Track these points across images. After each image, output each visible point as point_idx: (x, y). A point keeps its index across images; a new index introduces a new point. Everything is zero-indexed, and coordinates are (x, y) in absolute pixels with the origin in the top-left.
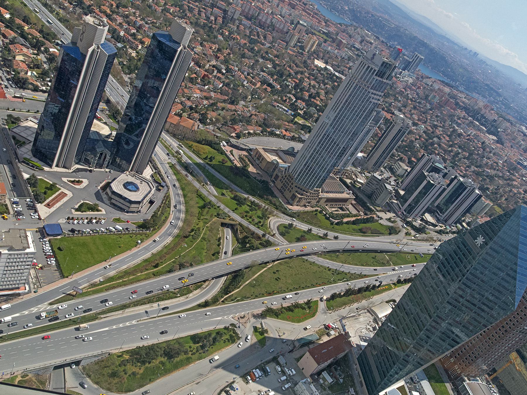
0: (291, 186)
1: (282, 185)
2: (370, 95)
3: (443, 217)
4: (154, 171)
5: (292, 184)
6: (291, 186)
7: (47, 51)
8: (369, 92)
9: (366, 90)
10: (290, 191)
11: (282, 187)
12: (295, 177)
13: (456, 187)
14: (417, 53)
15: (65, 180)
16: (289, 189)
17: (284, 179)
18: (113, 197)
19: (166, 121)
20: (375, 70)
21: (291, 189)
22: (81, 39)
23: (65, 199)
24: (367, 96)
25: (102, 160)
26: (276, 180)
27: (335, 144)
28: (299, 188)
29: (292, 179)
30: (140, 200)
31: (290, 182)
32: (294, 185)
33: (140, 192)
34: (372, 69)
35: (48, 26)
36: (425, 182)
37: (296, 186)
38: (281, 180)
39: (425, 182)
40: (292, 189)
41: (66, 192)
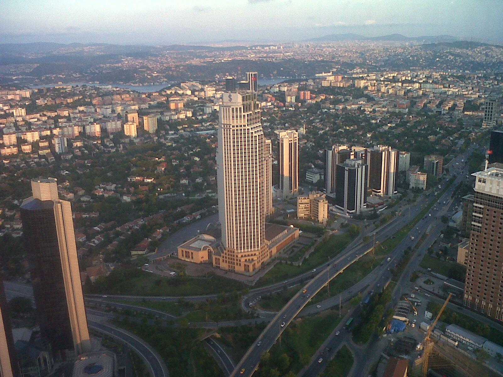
0: (237, 260)
2: (250, 131)
3: (382, 192)
4: (101, 339)
5: (237, 256)
9: (245, 130)
10: (240, 265)
11: (229, 266)
12: (235, 248)
13: (339, 159)
14: (248, 73)
16: (237, 264)
17: (226, 258)
19: (437, 295)
20: (240, 108)
21: (238, 262)
25: (43, 365)
27: (237, 117)
28: (245, 256)
29: (234, 252)
32: (239, 256)
33: (104, 369)
34: (237, 109)
36: (346, 173)
38: (223, 261)
39: (346, 173)
40: (240, 261)
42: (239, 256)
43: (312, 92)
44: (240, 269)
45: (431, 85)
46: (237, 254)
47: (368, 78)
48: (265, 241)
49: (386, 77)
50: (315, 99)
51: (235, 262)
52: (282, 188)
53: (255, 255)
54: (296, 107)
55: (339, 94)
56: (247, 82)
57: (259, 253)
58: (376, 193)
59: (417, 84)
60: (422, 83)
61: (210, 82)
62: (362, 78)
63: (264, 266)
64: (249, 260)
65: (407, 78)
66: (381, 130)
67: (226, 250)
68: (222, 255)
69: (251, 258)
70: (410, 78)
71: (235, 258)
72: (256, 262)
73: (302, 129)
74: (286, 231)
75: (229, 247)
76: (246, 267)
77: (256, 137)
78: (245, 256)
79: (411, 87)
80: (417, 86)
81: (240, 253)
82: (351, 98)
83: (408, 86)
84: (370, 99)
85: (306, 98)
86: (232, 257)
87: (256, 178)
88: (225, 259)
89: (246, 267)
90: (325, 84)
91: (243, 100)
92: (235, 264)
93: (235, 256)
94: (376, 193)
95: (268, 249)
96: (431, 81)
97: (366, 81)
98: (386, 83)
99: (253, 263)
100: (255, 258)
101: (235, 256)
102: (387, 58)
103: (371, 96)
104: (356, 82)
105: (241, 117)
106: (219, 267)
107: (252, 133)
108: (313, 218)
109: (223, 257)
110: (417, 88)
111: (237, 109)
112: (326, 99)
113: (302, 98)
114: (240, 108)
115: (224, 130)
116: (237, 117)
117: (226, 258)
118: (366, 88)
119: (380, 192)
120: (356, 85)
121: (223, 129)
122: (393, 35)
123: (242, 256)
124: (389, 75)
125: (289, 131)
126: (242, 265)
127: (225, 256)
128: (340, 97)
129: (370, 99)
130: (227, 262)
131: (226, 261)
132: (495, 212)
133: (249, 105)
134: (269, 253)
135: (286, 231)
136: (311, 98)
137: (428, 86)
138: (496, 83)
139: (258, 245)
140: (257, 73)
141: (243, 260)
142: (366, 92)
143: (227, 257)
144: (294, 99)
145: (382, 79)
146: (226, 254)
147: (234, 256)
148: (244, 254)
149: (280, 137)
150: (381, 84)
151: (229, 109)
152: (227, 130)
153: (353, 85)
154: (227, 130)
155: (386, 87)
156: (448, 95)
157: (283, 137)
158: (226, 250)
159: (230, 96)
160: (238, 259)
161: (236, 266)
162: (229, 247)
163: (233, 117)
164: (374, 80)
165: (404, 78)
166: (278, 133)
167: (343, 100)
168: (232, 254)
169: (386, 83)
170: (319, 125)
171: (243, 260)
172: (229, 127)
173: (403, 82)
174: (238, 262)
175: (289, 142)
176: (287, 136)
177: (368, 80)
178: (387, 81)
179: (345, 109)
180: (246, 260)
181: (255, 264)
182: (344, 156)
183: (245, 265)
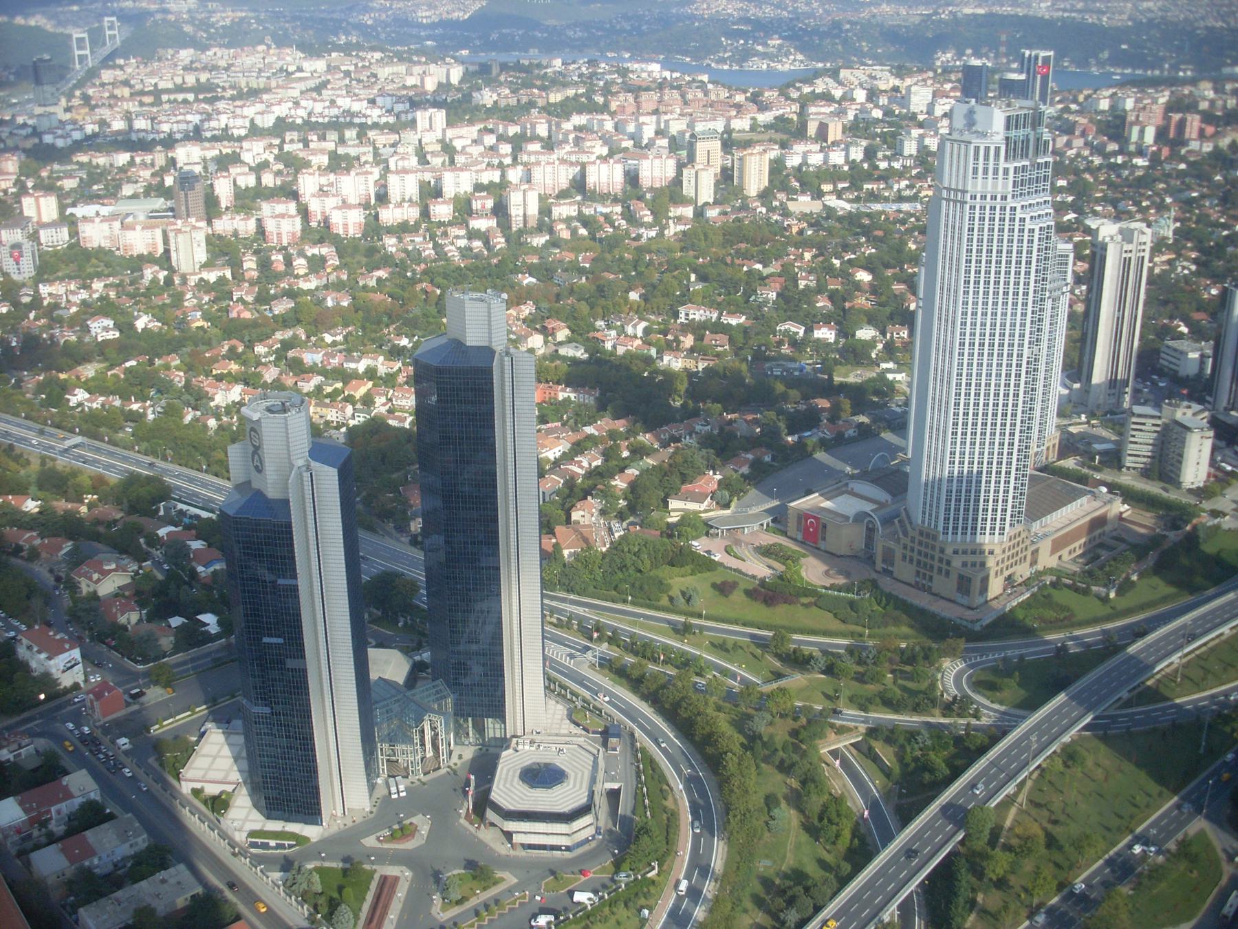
0: (941, 560)
1: (913, 568)
5: (942, 551)
6: (941, 560)
7: (153, 541)
8: (1013, 209)
10: (948, 573)
11: (918, 572)
12: (941, 529)
15: (370, 842)
16: (940, 570)
17: (912, 550)
18: (511, 826)
20: (998, 149)
21: (944, 566)
22: (256, 467)
23: (401, 893)
24: (1012, 220)
26: (892, 565)
27: (986, 171)
28: (965, 552)
30: (583, 800)
31: (919, 562)
32: (949, 551)
33: (572, 781)
34: (987, 149)
35: (148, 477)
37: (956, 552)
38: (904, 557)
40: (948, 563)
41: (392, 871)
43: (1208, 117)
51: (936, 564)
71: (937, 555)
87: (1021, 345)
88: (908, 553)
92: (935, 570)
93: (938, 549)
101: (938, 549)
109: (905, 547)
111: (987, 149)
114: (998, 149)
116: (986, 171)
126: (954, 576)
127: (910, 544)
131: (911, 560)
134: (1029, 553)
140: (1051, 53)
141: (957, 563)
143: (917, 547)
157: (1107, 239)
168: (931, 542)
174: (944, 566)
175: (1124, 255)
183: (961, 577)
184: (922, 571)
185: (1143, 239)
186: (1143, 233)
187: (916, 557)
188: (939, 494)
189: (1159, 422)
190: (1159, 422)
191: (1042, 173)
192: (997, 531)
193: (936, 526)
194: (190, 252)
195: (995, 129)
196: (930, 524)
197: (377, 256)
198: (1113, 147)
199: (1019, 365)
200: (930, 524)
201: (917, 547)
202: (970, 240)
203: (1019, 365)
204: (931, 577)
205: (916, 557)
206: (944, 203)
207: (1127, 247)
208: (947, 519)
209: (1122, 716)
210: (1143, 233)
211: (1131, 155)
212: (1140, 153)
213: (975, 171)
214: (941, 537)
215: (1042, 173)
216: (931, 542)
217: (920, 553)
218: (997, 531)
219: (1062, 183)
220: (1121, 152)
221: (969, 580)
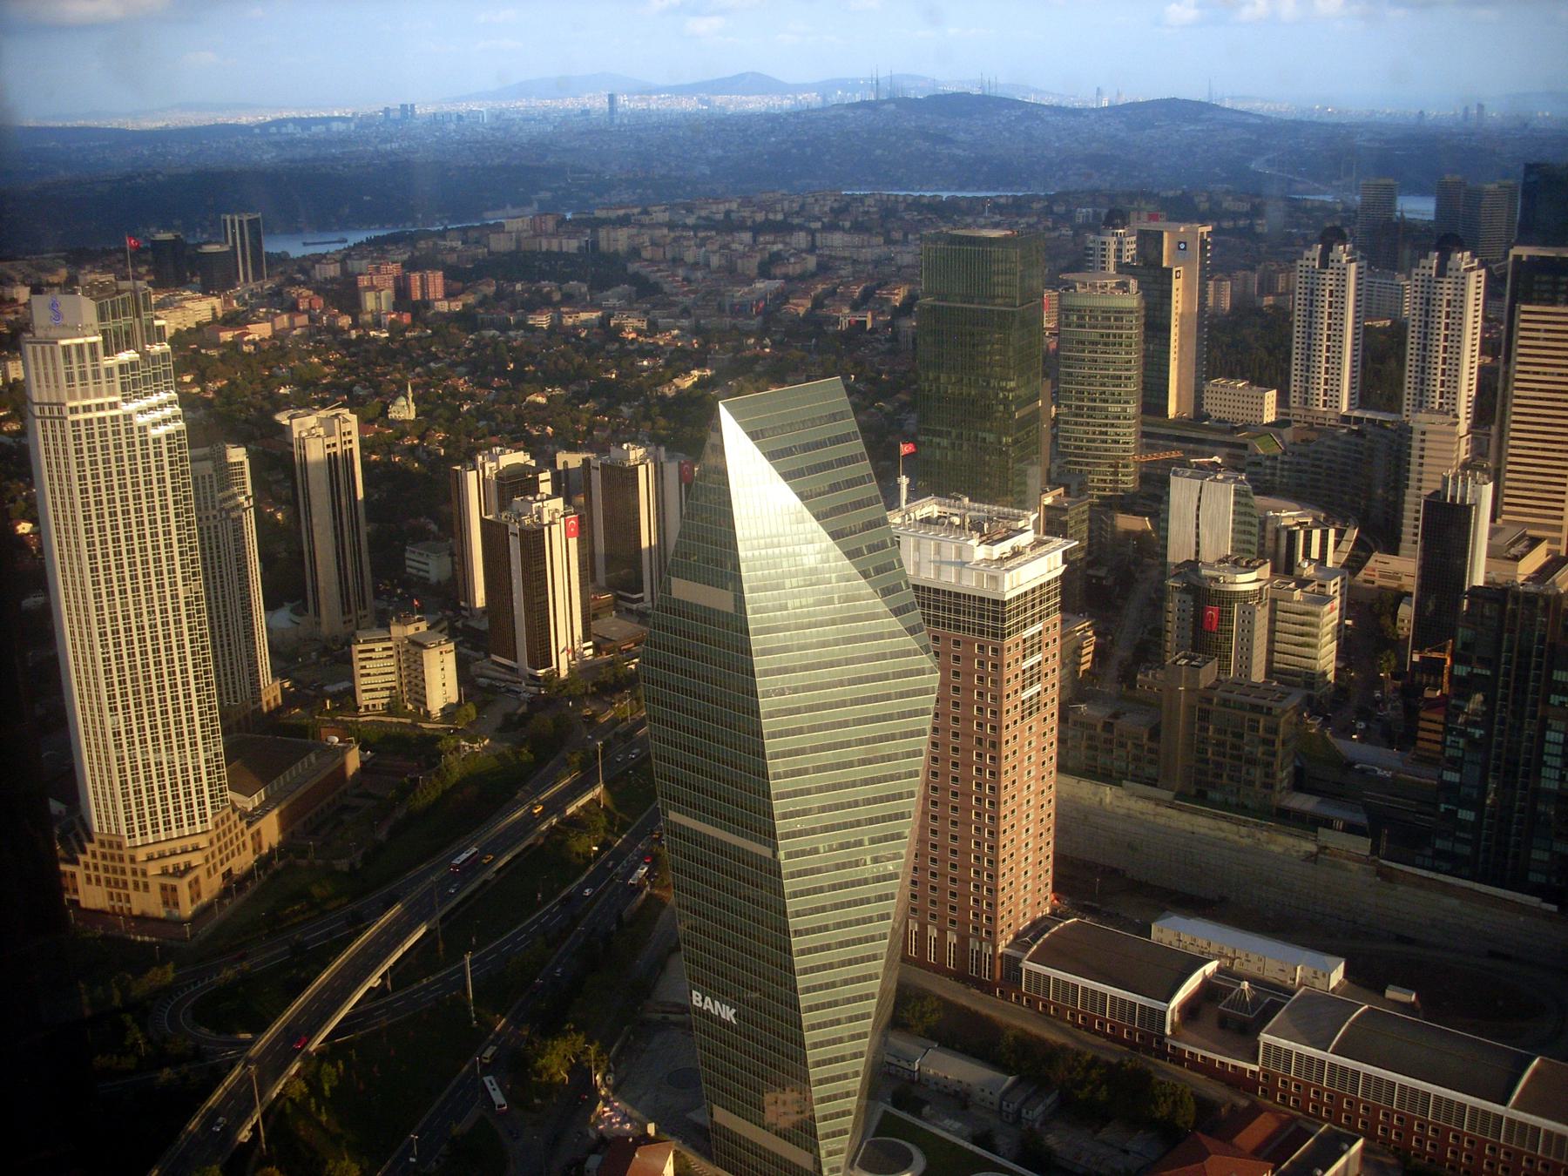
0: (134, 872)
3: (647, 597)
5: (133, 860)
10: (146, 886)
11: (111, 895)
12: (124, 832)
14: (228, 217)
16: (136, 885)
21: (140, 879)
27: (83, 376)
29: (120, 847)
32: (141, 855)
38: (89, 879)
40: (144, 874)
42: (141, 855)
44: (148, 903)
45: (847, 238)
46: (132, 852)
47: (646, 219)
48: (229, 794)
49: (703, 213)
50: (462, 296)
51: (130, 878)
52: (317, 613)
53: (196, 849)
54: (394, 328)
55: (544, 276)
56: (226, 248)
57: (211, 843)
58: (629, 605)
59: (803, 234)
60: (816, 230)
61: (108, 253)
62: (624, 222)
63: (234, 884)
64: (176, 867)
65: (771, 216)
66: (669, 391)
67: (91, 841)
68: (82, 858)
69: (181, 860)
70: (780, 217)
71: (128, 866)
72: (201, 873)
73: (402, 401)
74: (312, 757)
75: (101, 828)
76: (169, 894)
77: (157, 441)
78: (162, 856)
79: (780, 246)
80: (801, 239)
81: (141, 845)
82: (584, 289)
83: (774, 243)
84: (646, 291)
85: (432, 296)
86: (118, 864)
87: (173, 584)
88: (93, 873)
89: (169, 894)
90: (500, 244)
91: (102, 318)
92: (131, 885)
93: (127, 859)
94: (629, 605)
95: (244, 824)
96: (847, 224)
97: (634, 231)
98: (702, 234)
99: (190, 877)
100: (196, 859)
101: (127, 859)
102: (720, 152)
103: (654, 278)
104: (602, 233)
105: (96, 374)
106: (78, 902)
107: (143, 429)
108: (410, 707)
109: (87, 866)
110: (803, 246)
112: (500, 295)
113: (417, 295)
115: (43, 424)
116: (83, 376)
117: (96, 868)
118: (635, 253)
119: (641, 599)
120: (603, 245)
121: (38, 422)
122: (742, 76)
123: (150, 859)
124: (714, 208)
125: (323, 413)
127: (91, 862)
128: (546, 286)
129: (646, 291)
130: (103, 883)
131: (98, 880)
132: (957, 643)
133: (127, 333)
134: (248, 838)
135: (312, 757)
136: (450, 295)
137: (837, 239)
138: (1050, 224)
139: (203, 815)
141: (154, 869)
142: (633, 267)
143: (101, 863)
144: (387, 295)
145: (691, 221)
146: (94, 855)
147: (121, 859)
148: (155, 850)
149: (296, 435)
150: (687, 238)
151: (52, 350)
152: (53, 425)
153: (595, 244)
154: (53, 425)
155: (700, 246)
156: (899, 268)
158: (91, 841)
159: (54, 306)
160: (139, 867)
161: (133, 895)
162: (101, 828)
163: (70, 377)
164: (660, 225)
165: (760, 217)
166: (287, 422)
167: (557, 297)
168: (117, 852)
169: (702, 234)
170: (462, 385)
171: (154, 869)
172: (60, 411)
173: (757, 229)
174: (140, 879)
176: (321, 431)
177: (642, 226)
178: (706, 228)
179: (556, 328)
180: (165, 873)
181: (197, 880)
182: (515, 485)
183: (164, 888)
184: (115, 891)
185: (346, 428)
186: (346, 421)
187: (103, 875)
188: (112, 789)
189: (390, 644)
190: (390, 644)
191: (160, 368)
192: (173, 824)
193: (118, 830)
194: (1353, 266)
195: (86, 321)
196: (109, 829)
197: (427, 407)
198: (345, 321)
199: (176, 609)
200: (109, 829)
201: (101, 863)
202: (80, 464)
203: (176, 609)
204: (128, 896)
205: (103, 875)
206: (38, 422)
207: (331, 440)
208: (129, 819)
209: (378, 1009)
210: (346, 421)
211: (366, 327)
212: (378, 325)
213: (70, 377)
214: (127, 843)
215: (160, 368)
216: (117, 852)
217: (106, 869)
218: (173, 824)
219: (187, 379)
220: (355, 325)
221: (174, 889)
